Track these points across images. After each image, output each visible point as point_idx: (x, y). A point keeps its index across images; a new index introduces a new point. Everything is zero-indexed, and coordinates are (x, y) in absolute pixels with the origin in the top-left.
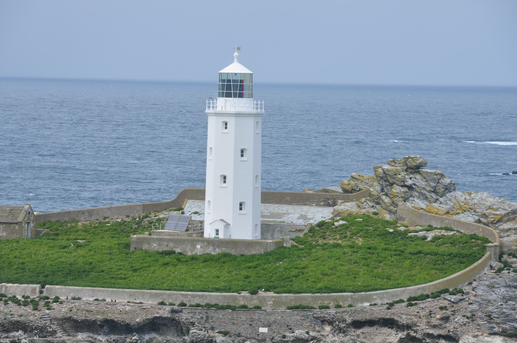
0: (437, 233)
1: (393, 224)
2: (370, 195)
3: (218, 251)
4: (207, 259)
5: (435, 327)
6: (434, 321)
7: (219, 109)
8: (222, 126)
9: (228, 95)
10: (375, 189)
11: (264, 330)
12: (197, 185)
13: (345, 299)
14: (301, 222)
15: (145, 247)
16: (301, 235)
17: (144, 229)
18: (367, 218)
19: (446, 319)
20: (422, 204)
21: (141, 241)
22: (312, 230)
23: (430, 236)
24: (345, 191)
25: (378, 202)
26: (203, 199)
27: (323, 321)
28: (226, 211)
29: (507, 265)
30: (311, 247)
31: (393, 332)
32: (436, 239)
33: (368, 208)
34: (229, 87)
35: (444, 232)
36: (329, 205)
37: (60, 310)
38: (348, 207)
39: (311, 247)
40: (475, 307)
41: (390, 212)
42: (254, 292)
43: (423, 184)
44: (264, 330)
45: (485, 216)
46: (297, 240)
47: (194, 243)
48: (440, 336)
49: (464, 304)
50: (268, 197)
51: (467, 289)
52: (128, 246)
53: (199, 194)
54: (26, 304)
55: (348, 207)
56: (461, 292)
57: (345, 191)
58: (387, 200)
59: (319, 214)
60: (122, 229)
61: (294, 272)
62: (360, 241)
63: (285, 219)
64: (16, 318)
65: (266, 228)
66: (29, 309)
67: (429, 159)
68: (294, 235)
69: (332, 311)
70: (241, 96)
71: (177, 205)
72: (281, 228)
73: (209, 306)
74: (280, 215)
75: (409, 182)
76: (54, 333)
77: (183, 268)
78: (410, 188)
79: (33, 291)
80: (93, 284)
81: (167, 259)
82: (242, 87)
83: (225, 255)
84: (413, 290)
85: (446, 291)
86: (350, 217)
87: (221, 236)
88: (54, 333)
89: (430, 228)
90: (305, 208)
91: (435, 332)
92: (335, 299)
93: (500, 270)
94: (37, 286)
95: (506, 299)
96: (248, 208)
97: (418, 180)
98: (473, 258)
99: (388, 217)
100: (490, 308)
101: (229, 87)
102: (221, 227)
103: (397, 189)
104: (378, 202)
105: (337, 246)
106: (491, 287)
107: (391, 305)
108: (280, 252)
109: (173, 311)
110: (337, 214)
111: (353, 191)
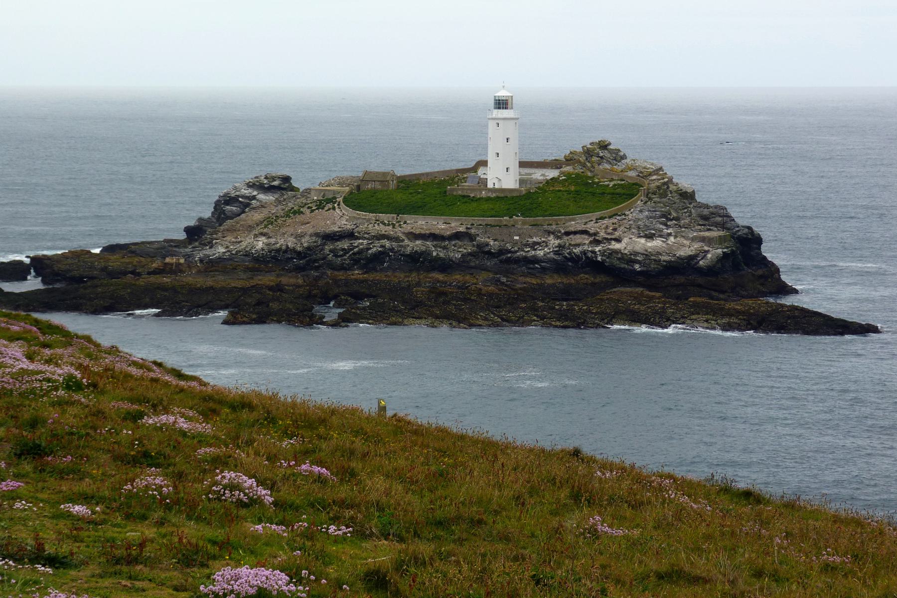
0: (615, 182)
1: (590, 178)
2: (580, 162)
3: (494, 195)
4: (488, 199)
5: (609, 234)
6: (610, 230)
7: (494, 116)
8: (496, 125)
9: (499, 108)
10: (582, 159)
11: (516, 238)
12: (483, 158)
13: (560, 220)
14: (542, 178)
15: (455, 193)
16: (541, 185)
17: (455, 183)
18: (577, 175)
19: (615, 230)
20: (608, 166)
21: (452, 190)
22: (548, 182)
23: (612, 184)
24: (567, 160)
25: (584, 165)
26: (487, 166)
27: (549, 233)
28: (501, 175)
29: (650, 199)
30: (546, 192)
31: (587, 237)
32: (615, 185)
33: (579, 170)
34: (499, 104)
35: (619, 182)
36: (558, 168)
37: (408, 228)
38: (568, 169)
39: (546, 192)
40: (631, 222)
41: (591, 171)
42: (511, 217)
43: (609, 155)
44: (516, 238)
45: (641, 172)
46: (539, 188)
47: (481, 191)
48: (611, 239)
49: (625, 221)
50: (523, 164)
51: (627, 213)
52: (445, 192)
53: (484, 163)
54: (389, 225)
55: (568, 169)
56: (625, 214)
57: (567, 160)
58: (589, 165)
59: (552, 174)
60: (442, 183)
61: (535, 206)
62: (573, 188)
63: (533, 176)
64: (383, 232)
65: (522, 182)
66: (390, 228)
67: (612, 141)
68: (537, 186)
69: (554, 227)
70: (506, 108)
71: (474, 169)
72: (531, 181)
73: (487, 225)
74: (530, 174)
75: (601, 154)
76: (403, 240)
77: (475, 205)
78: (602, 158)
79: (393, 218)
80: (424, 213)
81: (465, 199)
82: (507, 104)
83: (498, 197)
84: (598, 214)
85: (616, 214)
86: (568, 175)
87: (496, 187)
88: (403, 240)
89: (612, 180)
90: (545, 170)
91: (609, 237)
92: (555, 220)
93: (646, 202)
94: (395, 215)
95: (648, 218)
96: (511, 170)
97: (606, 154)
98: (632, 196)
99: (589, 174)
100: (640, 223)
101: (499, 104)
102: (496, 181)
103: (595, 159)
104: (584, 165)
105: (560, 191)
106: (641, 211)
107: (586, 223)
108: (529, 195)
109: (467, 228)
110: (562, 173)
111: (571, 160)
